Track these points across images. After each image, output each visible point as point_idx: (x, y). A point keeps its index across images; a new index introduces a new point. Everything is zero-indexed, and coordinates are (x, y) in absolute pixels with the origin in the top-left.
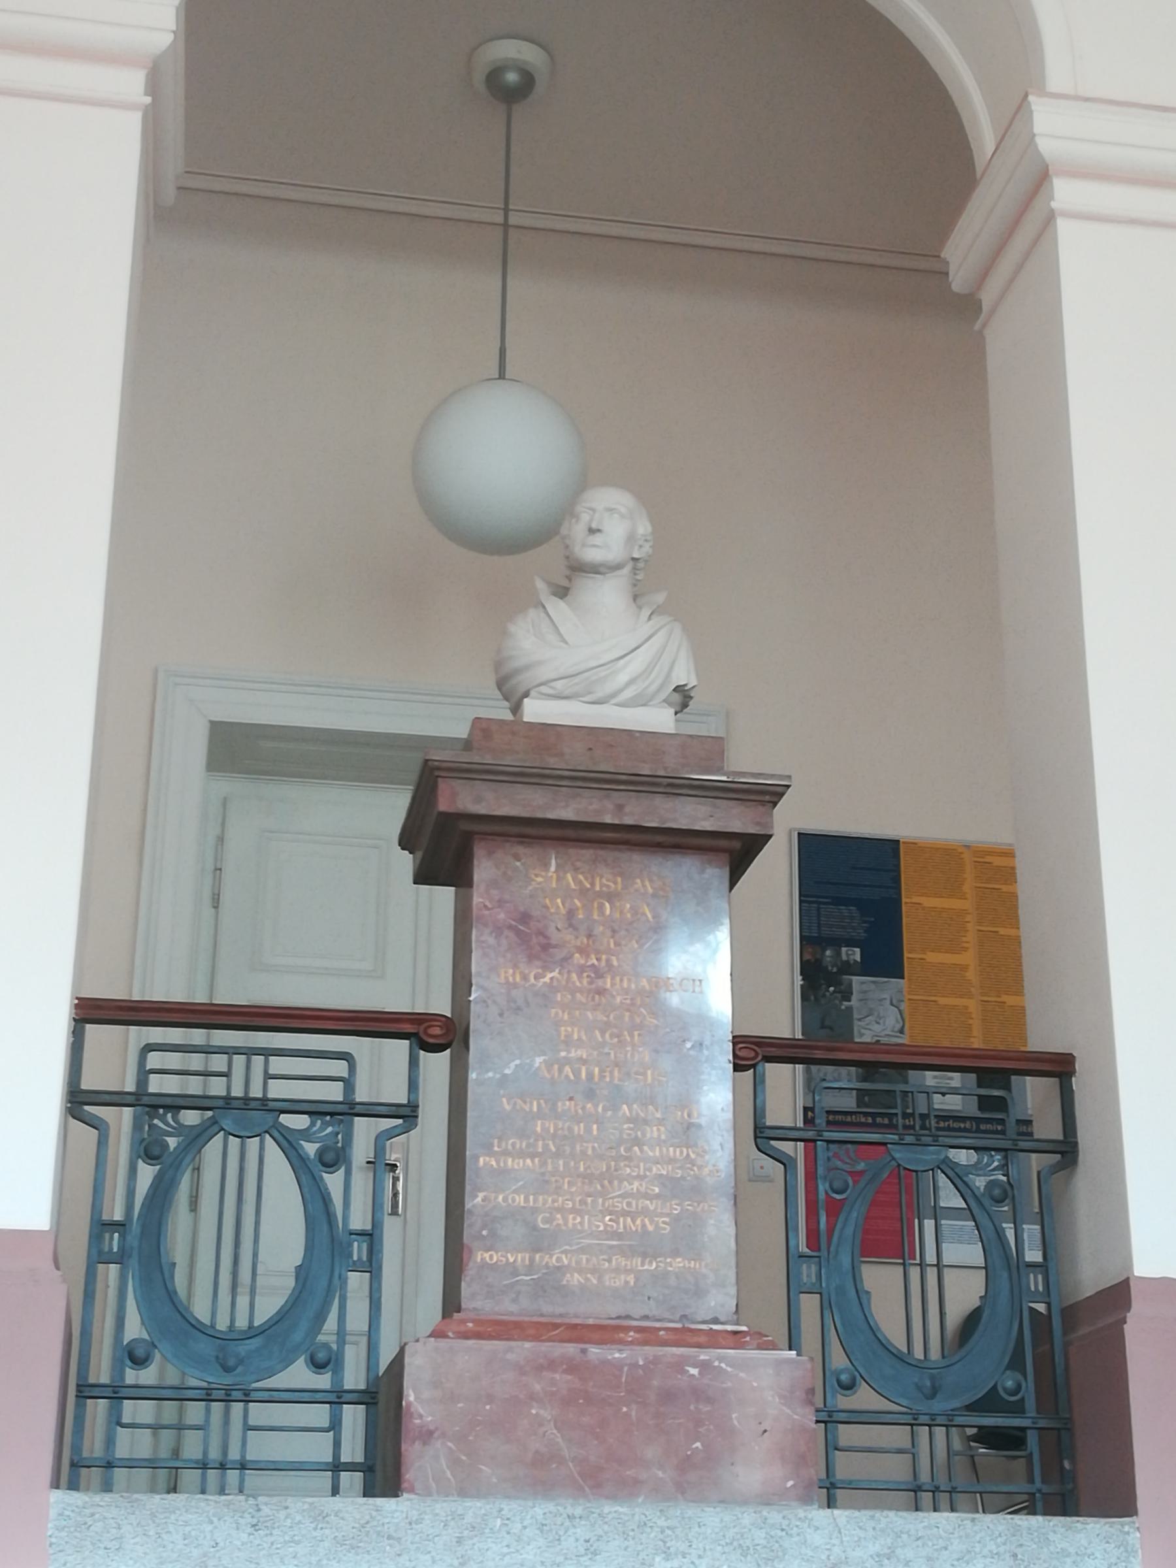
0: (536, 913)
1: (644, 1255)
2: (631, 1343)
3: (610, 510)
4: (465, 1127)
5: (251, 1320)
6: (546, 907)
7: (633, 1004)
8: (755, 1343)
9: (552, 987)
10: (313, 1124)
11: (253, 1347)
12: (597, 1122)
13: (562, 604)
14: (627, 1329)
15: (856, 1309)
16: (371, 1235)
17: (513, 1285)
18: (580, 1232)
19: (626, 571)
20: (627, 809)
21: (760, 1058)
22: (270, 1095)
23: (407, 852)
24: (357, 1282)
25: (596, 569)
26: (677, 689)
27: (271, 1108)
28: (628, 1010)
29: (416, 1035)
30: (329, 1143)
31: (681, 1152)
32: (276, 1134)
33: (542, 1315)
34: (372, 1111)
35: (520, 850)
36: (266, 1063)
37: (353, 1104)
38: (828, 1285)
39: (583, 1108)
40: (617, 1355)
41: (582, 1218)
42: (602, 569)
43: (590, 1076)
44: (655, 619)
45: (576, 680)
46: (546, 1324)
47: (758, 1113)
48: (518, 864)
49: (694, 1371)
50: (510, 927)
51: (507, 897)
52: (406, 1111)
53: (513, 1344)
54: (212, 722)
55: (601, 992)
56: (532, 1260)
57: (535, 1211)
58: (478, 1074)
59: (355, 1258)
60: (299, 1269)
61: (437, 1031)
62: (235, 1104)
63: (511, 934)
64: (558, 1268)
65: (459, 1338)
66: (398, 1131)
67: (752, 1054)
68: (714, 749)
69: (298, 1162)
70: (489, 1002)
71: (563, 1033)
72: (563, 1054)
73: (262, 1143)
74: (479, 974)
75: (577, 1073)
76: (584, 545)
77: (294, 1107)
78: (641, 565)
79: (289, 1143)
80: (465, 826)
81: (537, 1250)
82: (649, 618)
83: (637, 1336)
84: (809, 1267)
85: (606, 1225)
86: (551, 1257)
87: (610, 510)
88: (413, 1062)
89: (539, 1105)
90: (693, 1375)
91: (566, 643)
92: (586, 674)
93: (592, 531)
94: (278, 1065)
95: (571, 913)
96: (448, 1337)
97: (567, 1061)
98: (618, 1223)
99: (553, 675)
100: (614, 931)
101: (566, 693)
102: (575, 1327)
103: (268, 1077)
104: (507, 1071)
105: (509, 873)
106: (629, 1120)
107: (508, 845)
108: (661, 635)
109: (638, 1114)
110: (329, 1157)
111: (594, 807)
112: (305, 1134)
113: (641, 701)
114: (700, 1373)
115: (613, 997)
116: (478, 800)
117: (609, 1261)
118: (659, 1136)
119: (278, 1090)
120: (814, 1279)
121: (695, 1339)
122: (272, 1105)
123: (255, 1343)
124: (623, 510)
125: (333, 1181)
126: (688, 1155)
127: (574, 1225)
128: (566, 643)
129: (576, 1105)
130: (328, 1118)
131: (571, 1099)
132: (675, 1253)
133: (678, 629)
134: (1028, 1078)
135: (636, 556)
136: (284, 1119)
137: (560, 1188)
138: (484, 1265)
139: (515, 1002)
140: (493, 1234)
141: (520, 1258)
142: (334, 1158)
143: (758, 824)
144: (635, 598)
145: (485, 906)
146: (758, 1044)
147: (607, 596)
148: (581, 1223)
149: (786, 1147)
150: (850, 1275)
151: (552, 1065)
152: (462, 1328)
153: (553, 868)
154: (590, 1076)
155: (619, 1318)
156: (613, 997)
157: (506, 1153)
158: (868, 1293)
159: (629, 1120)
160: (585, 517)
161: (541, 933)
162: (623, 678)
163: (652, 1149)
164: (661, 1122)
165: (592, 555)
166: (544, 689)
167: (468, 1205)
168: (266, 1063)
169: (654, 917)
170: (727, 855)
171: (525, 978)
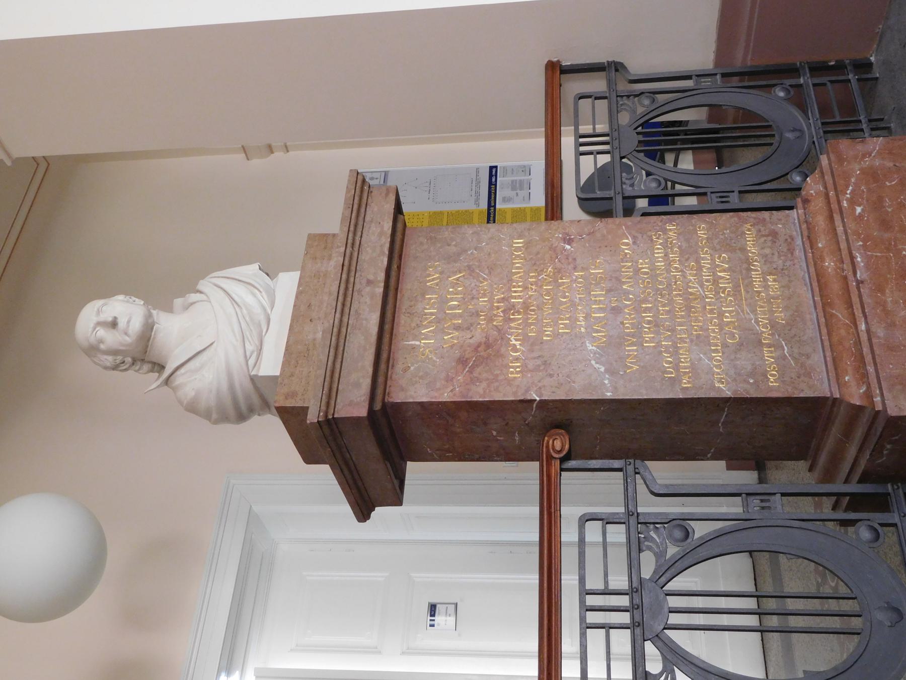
0: (457, 353)
1: (749, 270)
4: (659, 399)
6: (452, 347)
7: (536, 283)
9: (525, 339)
10: (649, 548)
17: (794, 358)
18: (738, 313)
20: (371, 277)
23: (373, 514)
25: (149, 328)
27: (635, 590)
28: (541, 287)
32: (663, 579)
40: (859, 259)
41: (725, 312)
43: (600, 310)
45: (247, 333)
48: (412, 368)
49: (859, 210)
50: (470, 372)
51: (443, 375)
55: (526, 306)
56: (769, 346)
57: (725, 345)
58: (607, 391)
62: (638, 618)
63: (478, 370)
64: (772, 327)
68: (319, 243)
70: (540, 384)
72: (583, 330)
74: (515, 393)
77: (633, 565)
79: (670, 569)
81: (760, 343)
85: (728, 295)
86: (763, 332)
90: (862, 210)
91: (212, 344)
95: (457, 328)
98: (725, 288)
99: (241, 351)
100: (473, 298)
101: (257, 343)
104: (603, 369)
105: (421, 374)
107: (394, 376)
111: (368, 300)
114: (859, 206)
116: (357, 385)
117: (759, 292)
119: (619, 581)
125: (700, 530)
127: (732, 317)
132: (743, 250)
134: (541, 142)
137: (701, 327)
138: (781, 378)
139: (539, 366)
140: (752, 374)
141: (769, 356)
145: (452, 391)
148: (730, 312)
153: (418, 343)
157: (677, 368)
161: (476, 348)
166: (251, 362)
167: (729, 394)
169: (460, 272)
171: (517, 359)
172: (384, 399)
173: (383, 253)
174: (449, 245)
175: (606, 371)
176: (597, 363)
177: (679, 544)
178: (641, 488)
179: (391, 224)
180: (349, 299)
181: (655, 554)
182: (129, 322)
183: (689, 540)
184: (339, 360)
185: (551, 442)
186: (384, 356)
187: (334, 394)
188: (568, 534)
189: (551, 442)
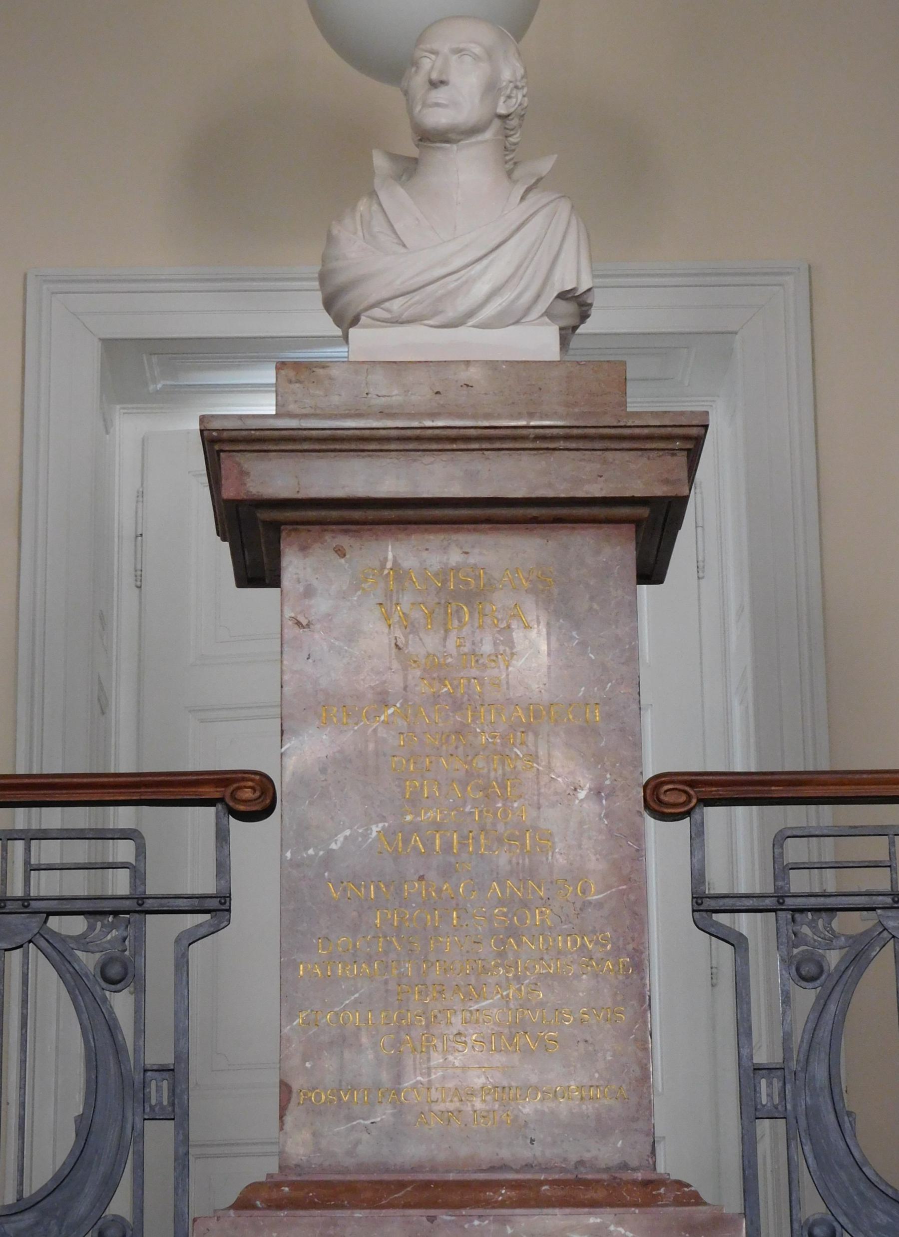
2: (502, 1205)
3: (459, 51)
5: (20, 1192)
8: (671, 1196)
10: (92, 928)
11: (22, 1225)
12: (457, 908)
13: (400, 191)
14: (499, 1184)
15: (835, 1135)
16: (173, 1070)
19: (488, 135)
21: (694, 801)
22: (33, 893)
24: (158, 1138)
26: (563, 296)
29: (221, 800)
30: (116, 952)
31: (574, 942)
33: (387, 1171)
34: (170, 906)
35: (344, 541)
36: (28, 849)
37: (141, 899)
38: (795, 1107)
39: (439, 891)
42: (453, 136)
43: (447, 848)
44: (532, 197)
45: (417, 297)
46: (388, 1183)
47: (698, 877)
52: (214, 904)
53: (338, 1213)
54: (104, 341)
59: (153, 1102)
60: (79, 1120)
61: (247, 794)
65: (269, 1207)
66: (204, 931)
67: (683, 798)
69: (74, 981)
71: (409, 790)
72: (409, 818)
73: (26, 956)
75: (429, 843)
76: (425, 105)
77: (66, 907)
78: (514, 122)
79: (60, 954)
80: (265, 515)
82: (523, 198)
83: (513, 1194)
84: (770, 1084)
87: (458, 51)
88: (222, 837)
89: (377, 888)
91: (404, 246)
92: (429, 289)
93: (434, 84)
94: (49, 852)
96: (254, 1207)
97: (416, 828)
99: (385, 294)
101: (405, 316)
102: (426, 1185)
103: (30, 868)
104: (333, 846)
106: (501, 903)
108: (539, 219)
109: (513, 893)
110: (114, 971)
112: (82, 942)
113: (513, 317)
115: (476, 735)
118: (543, 921)
119: (46, 885)
120: (776, 1101)
121: (591, 1195)
122: (35, 905)
123: (28, 1219)
124: (477, 50)
125: (121, 1004)
126: (583, 945)
128: (404, 246)
129: (428, 887)
130: (111, 918)
131: (421, 878)
133: (564, 208)
135: (502, 110)
136: (54, 922)
142: (121, 973)
143: (666, 482)
144: (509, 173)
146: (692, 784)
147: (466, 171)
149: (744, 923)
150: (827, 1092)
151: (394, 833)
152: (274, 1195)
154: (447, 848)
155: (492, 1169)
156: (476, 735)
158: (849, 1114)
159: (501, 903)
160: (426, 64)
162: (482, 288)
163: (533, 939)
164: (546, 902)
165: (437, 119)
166: (377, 312)
168: (28, 849)
170: (632, 527)
172: (286, 523)
173: (587, 493)
174: (592, 598)
175: (330, 853)
176: (346, 838)
177: (98, 970)
178: (191, 921)
179: (598, 494)
180: (581, 445)
181: (84, 936)
182: (437, 105)
183: (104, 984)
184: (317, 447)
185: (250, 784)
186: (357, 514)
187: (257, 447)
188: (123, 817)
189: (250, 784)
